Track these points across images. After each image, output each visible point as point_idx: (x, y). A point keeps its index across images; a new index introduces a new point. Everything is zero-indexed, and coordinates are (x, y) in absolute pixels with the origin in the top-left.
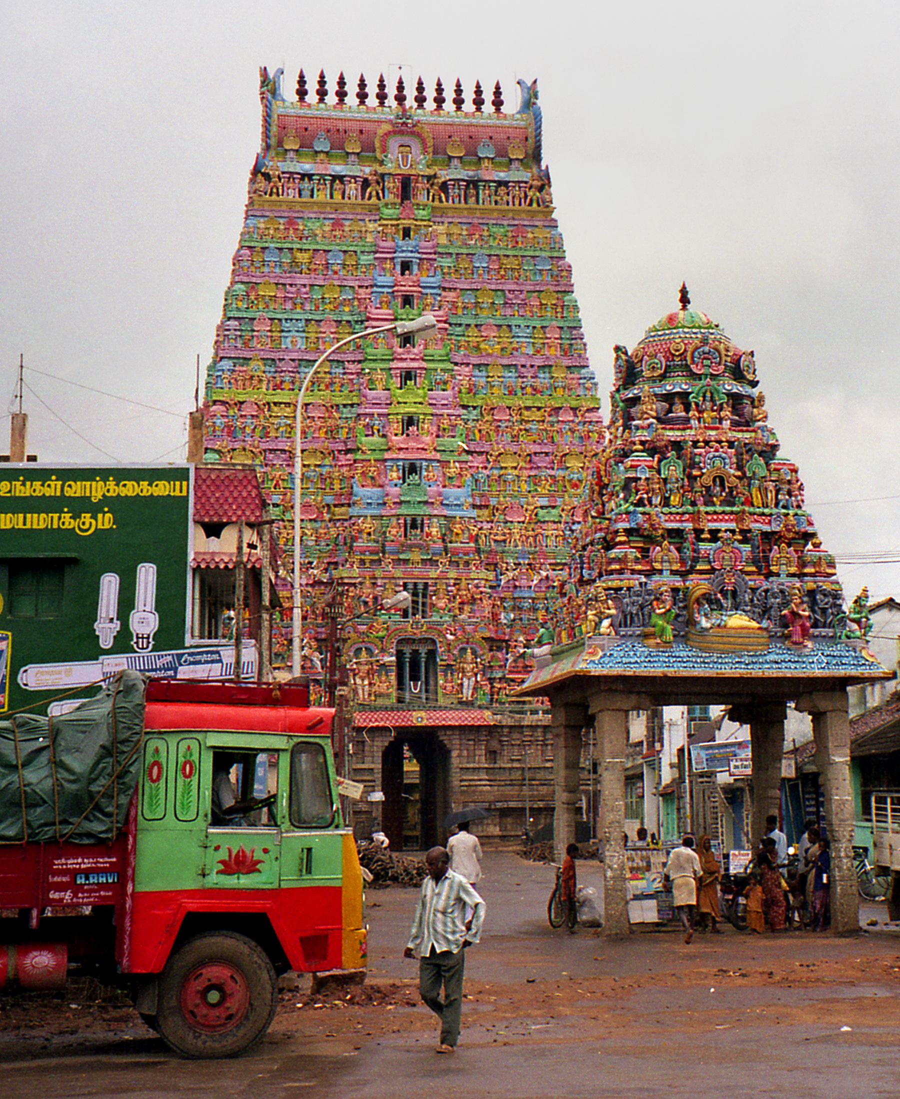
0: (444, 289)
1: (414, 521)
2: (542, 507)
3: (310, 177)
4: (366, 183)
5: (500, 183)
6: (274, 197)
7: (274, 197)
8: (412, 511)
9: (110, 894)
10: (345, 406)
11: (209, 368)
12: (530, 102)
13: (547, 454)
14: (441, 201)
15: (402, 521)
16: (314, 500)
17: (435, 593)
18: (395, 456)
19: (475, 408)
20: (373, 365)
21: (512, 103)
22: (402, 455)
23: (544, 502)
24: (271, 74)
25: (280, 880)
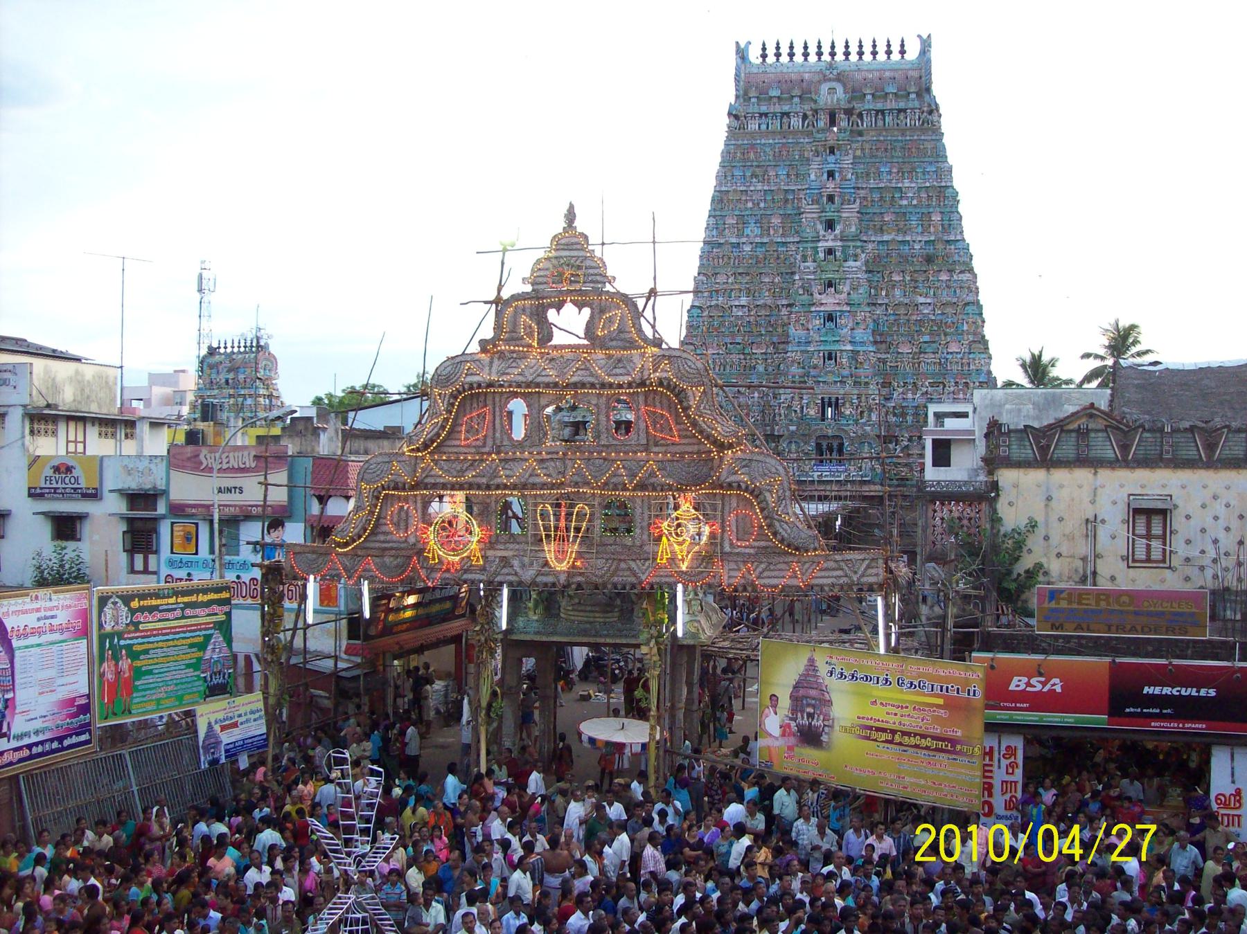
0: (858, 188)
1: (830, 354)
2: (925, 342)
3: (766, 115)
4: (805, 117)
5: (900, 111)
6: (742, 131)
7: (742, 131)
8: (828, 348)
9: (1146, 690)
10: (787, 273)
11: (688, 311)
12: (926, 45)
13: (930, 304)
14: (858, 125)
15: (821, 355)
16: (840, 130)
17: (844, 404)
18: (818, 309)
19: (878, 272)
20: (805, 245)
21: (913, 53)
22: (822, 308)
23: (926, 338)
24: (742, 46)
25: (1148, 560)
